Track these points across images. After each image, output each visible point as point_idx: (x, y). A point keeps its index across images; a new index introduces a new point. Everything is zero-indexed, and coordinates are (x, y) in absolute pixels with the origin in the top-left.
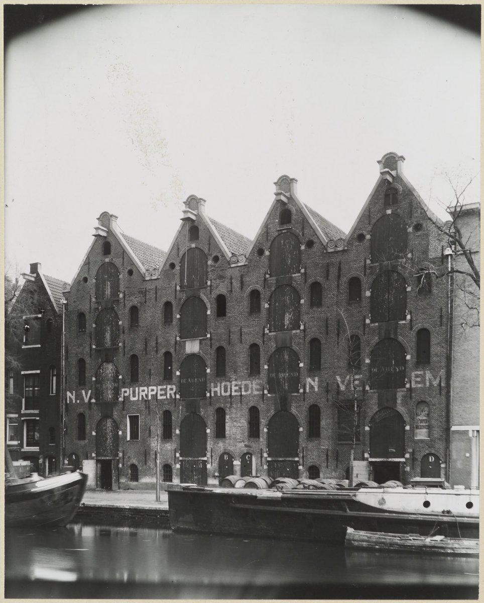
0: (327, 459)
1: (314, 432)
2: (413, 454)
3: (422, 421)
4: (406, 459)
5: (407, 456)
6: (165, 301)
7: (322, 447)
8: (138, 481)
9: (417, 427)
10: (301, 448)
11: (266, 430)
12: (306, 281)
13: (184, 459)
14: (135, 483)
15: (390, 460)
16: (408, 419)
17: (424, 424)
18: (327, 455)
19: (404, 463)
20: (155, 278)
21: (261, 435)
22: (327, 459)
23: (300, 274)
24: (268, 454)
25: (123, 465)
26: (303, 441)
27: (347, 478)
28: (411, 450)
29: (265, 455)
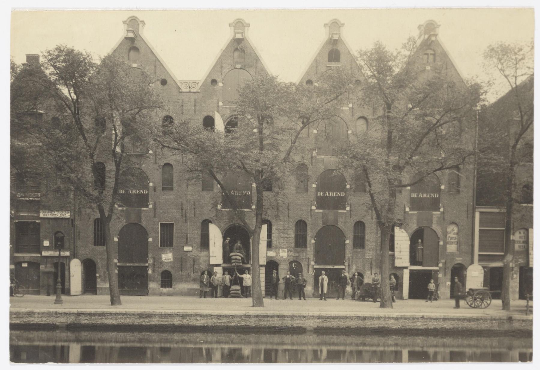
0: (371, 268)
1: (360, 242)
2: (445, 263)
3: (452, 238)
4: (440, 268)
5: (441, 265)
6: (206, 115)
7: (367, 257)
8: (171, 287)
9: (448, 243)
10: (347, 258)
11: (313, 241)
12: (353, 115)
13: (124, 264)
14: (168, 289)
15: (336, 267)
16: (442, 236)
17: (453, 241)
18: (371, 264)
19: (438, 271)
20: (195, 91)
21: (308, 245)
22: (371, 268)
23: (229, 284)
24: (315, 263)
25: (153, 271)
26: (349, 253)
27: (496, 296)
28: (443, 261)
29: (313, 263)
